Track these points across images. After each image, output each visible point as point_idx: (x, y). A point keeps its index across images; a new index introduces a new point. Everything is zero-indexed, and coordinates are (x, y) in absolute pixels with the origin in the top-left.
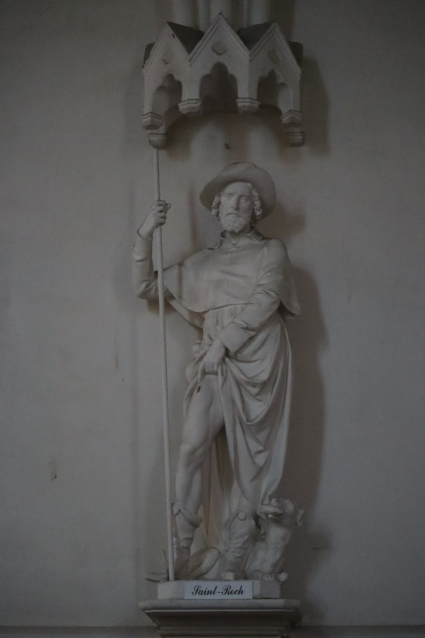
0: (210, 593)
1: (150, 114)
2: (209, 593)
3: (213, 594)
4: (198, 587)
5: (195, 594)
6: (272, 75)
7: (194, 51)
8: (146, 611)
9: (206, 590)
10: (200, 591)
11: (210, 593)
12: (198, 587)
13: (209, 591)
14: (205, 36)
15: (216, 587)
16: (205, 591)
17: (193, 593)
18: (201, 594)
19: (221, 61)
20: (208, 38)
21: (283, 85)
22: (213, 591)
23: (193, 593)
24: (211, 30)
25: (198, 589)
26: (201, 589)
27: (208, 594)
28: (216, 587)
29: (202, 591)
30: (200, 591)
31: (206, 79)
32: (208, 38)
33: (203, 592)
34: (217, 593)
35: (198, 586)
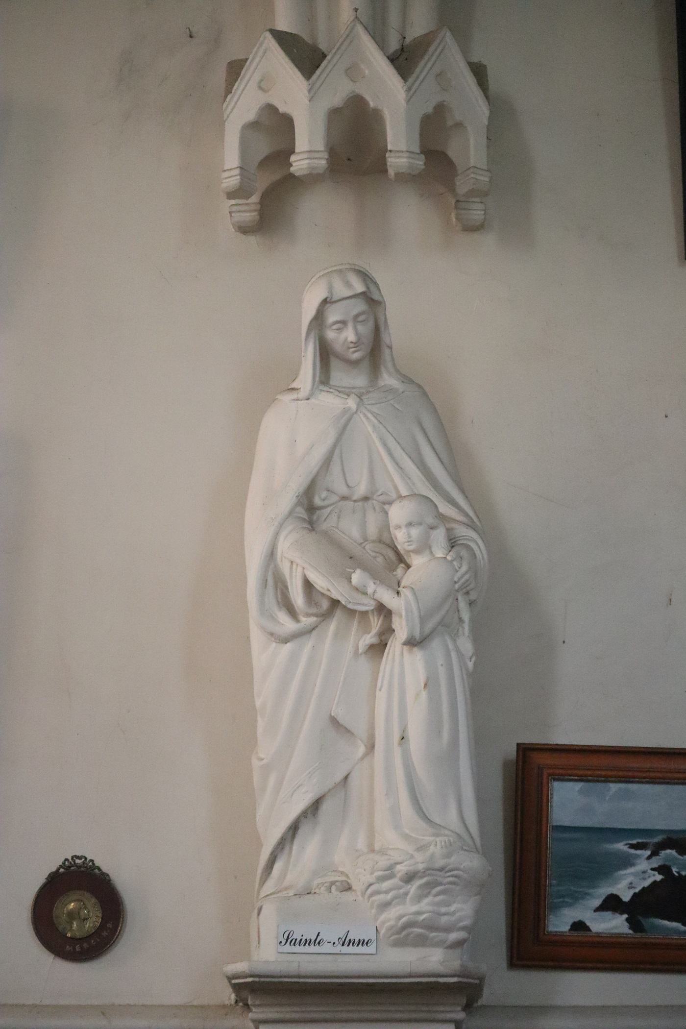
0: (308, 942)
1: (407, 154)
2: (351, 944)
3: (298, 944)
4: (290, 933)
5: (285, 944)
6: (440, 109)
7: (314, 77)
8: (234, 981)
9: (302, 938)
10: (292, 940)
11: (308, 942)
12: (290, 933)
13: (306, 940)
14: (328, 57)
15: (319, 933)
16: (301, 940)
17: (281, 942)
18: (294, 944)
19: (358, 91)
20: (434, 57)
21: (459, 125)
22: (312, 941)
23: (281, 942)
24: (436, 50)
25: (290, 937)
26: (295, 937)
27: (305, 945)
28: (319, 933)
29: (296, 939)
30: (292, 940)
31: (334, 114)
32: (434, 57)
33: (297, 942)
34: (326, 942)
35: (289, 932)
